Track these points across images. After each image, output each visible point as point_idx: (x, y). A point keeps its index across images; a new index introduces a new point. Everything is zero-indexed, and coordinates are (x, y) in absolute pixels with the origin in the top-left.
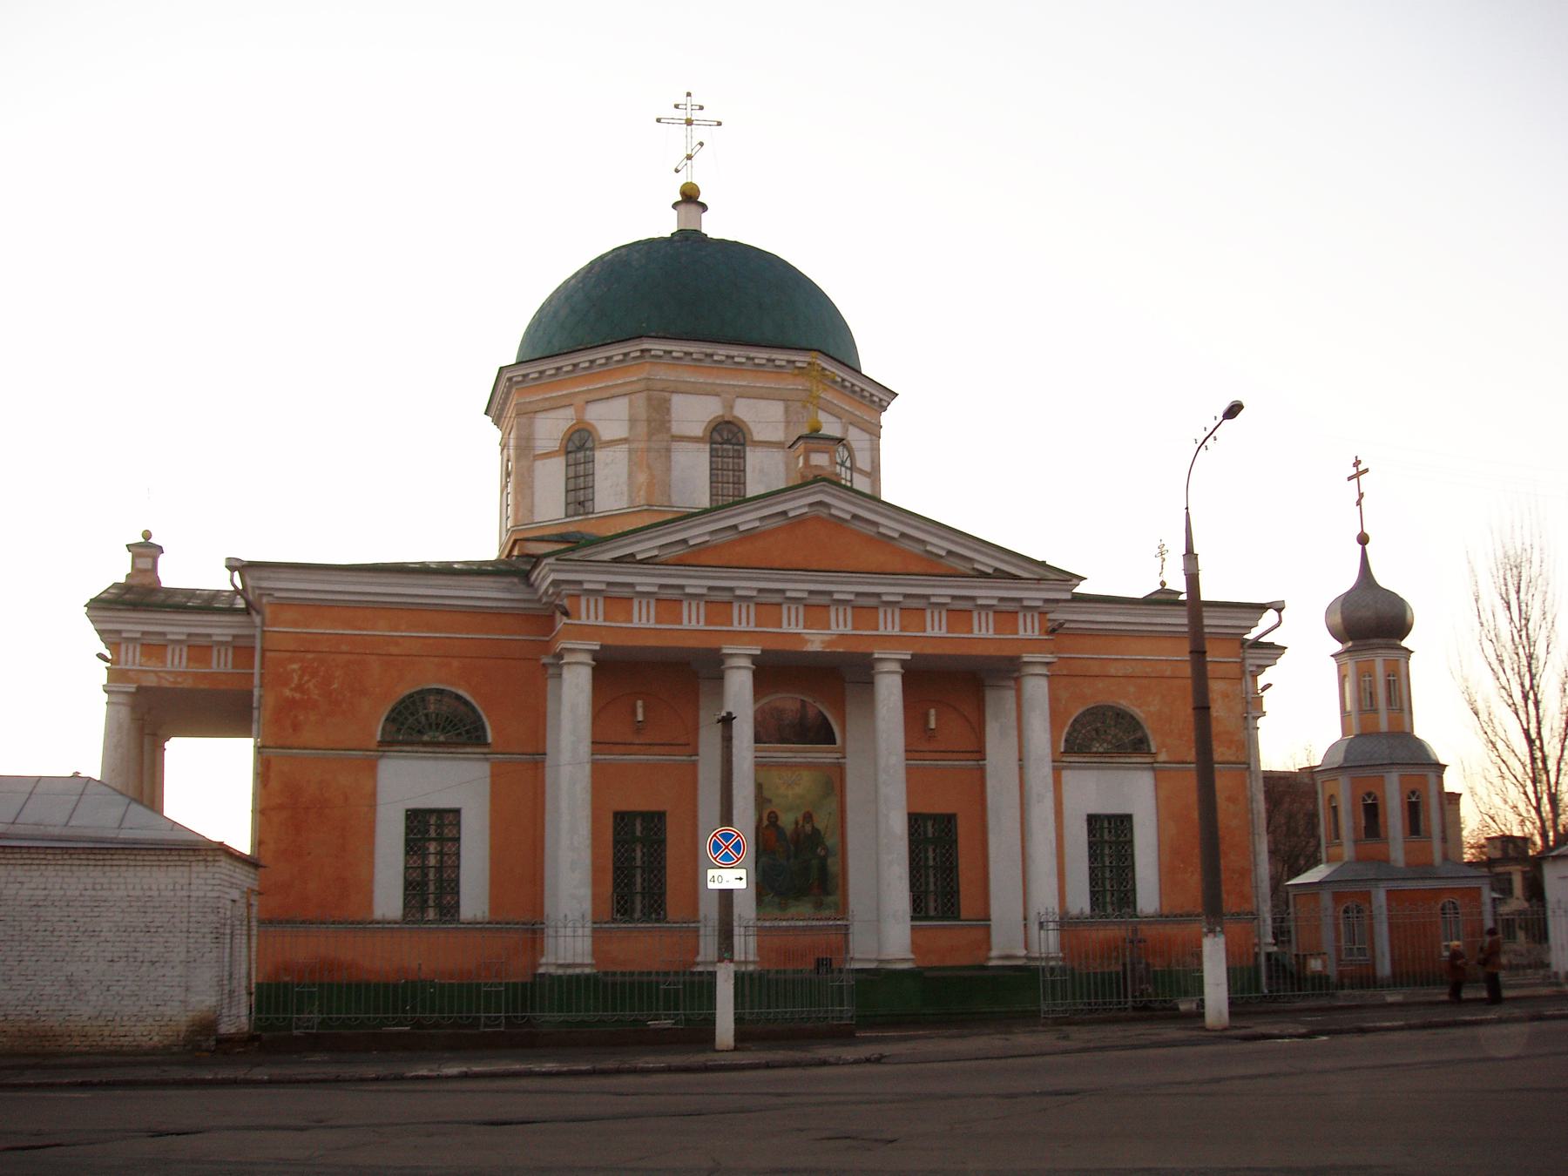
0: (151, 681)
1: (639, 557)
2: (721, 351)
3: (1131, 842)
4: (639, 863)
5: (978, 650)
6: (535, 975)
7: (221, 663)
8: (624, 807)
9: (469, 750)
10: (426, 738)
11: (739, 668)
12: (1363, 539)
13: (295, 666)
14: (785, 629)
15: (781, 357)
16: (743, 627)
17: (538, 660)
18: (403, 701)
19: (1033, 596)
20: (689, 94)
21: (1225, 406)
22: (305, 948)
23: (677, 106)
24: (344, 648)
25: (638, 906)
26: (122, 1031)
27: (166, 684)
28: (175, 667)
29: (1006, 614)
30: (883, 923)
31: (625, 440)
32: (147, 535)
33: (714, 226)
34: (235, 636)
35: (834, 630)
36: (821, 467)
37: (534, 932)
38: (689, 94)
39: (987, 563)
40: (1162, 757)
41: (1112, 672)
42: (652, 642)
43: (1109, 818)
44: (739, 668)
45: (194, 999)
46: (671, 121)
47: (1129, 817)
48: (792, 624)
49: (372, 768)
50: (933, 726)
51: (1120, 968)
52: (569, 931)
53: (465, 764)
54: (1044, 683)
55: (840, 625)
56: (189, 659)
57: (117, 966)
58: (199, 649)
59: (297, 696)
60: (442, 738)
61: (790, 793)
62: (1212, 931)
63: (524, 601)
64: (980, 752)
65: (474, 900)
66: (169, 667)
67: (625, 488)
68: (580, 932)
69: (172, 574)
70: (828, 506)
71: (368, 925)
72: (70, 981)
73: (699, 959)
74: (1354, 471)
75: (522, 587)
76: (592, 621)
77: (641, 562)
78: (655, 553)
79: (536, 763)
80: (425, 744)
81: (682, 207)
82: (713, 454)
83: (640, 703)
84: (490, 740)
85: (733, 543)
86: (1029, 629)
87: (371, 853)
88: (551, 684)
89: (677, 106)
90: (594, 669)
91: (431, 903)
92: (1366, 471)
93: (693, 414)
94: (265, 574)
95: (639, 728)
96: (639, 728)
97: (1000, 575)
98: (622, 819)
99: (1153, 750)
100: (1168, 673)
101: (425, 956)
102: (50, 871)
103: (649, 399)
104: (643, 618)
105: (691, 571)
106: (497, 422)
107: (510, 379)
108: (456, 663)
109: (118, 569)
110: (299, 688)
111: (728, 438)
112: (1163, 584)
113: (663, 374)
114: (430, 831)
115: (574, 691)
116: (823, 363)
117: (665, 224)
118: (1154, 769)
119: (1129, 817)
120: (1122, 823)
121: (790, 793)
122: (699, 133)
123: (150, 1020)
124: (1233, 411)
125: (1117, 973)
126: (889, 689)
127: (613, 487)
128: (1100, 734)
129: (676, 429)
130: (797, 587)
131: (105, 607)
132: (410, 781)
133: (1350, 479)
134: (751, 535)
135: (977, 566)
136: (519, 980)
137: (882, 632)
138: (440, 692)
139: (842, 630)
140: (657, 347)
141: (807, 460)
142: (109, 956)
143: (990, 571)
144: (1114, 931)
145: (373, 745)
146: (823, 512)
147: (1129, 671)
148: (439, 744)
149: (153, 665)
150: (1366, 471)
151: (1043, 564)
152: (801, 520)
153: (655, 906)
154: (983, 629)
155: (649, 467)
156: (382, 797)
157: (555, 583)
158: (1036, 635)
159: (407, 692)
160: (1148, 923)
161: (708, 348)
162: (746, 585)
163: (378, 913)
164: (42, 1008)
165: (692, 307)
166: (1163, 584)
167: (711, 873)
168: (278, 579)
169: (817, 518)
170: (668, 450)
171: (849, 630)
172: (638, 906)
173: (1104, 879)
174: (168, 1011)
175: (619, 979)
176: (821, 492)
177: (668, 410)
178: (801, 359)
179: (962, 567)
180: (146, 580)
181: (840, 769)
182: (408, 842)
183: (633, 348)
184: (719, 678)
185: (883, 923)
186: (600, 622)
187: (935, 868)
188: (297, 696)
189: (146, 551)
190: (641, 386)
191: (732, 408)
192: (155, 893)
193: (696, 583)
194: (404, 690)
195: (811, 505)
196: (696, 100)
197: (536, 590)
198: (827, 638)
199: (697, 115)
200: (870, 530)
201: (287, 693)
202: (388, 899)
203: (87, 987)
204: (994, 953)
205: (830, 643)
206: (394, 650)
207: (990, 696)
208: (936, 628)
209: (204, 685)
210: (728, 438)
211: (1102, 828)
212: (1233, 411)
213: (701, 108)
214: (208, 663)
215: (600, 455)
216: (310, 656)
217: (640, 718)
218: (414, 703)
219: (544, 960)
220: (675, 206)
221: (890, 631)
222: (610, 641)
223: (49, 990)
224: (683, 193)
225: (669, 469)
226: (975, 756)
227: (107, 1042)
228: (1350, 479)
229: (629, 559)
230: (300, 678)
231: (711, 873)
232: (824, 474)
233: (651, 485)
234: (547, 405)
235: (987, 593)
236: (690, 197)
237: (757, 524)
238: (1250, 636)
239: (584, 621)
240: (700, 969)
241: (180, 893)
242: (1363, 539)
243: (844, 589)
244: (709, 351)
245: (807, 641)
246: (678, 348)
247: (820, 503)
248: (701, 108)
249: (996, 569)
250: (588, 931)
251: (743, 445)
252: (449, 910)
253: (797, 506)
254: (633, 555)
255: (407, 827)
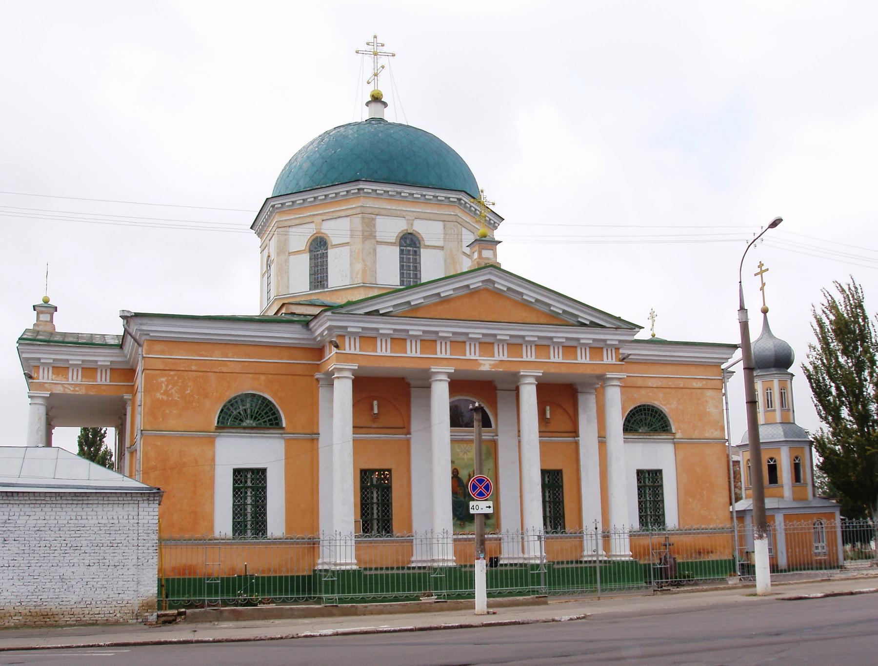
0: (58, 390)
1: (381, 312)
2: (406, 191)
3: (662, 486)
4: (375, 500)
5: (580, 371)
6: (314, 571)
7: (103, 379)
8: (366, 467)
9: (271, 431)
10: (244, 424)
11: (440, 380)
12: (765, 311)
13: (163, 379)
14: (468, 357)
15: (442, 195)
16: (443, 356)
17: (313, 376)
18: (230, 401)
19: (613, 338)
20: (375, 37)
21: (771, 220)
22: (183, 558)
23: (368, 44)
24: (194, 368)
25: (375, 527)
26: (97, 611)
27: (69, 392)
28: (73, 383)
29: (597, 349)
30: (525, 536)
31: (442, 248)
32: (46, 301)
33: (390, 115)
34: (111, 362)
35: (497, 358)
36: (488, 259)
37: (313, 545)
38: (375, 37)
39: (585, 318)
40: (678, 435)
41: (650, 385)
42: (389, 364)
43: (649, 471)
44: (440, 380)
45: (142, 589)
46: (364, 53)
47: (660, 471)
48: (472, 354)
49: (212, 441)
50: (548, 416)
51: (731, 558)
52: (343, 542)
53: (270, 441)
54: (617, 391)
55: (501, 354)
56: (82, 377)
57: (93, 569)
58: (89, 370)
59: (165, 398)
60: (254, 424)
61: (465, 457)
62: (761, 537)
63: (304, 339)
64: (575, 432)
65: (276, 522)
66: (70, 382)
67: (348, 273)
68: (349, 543)
69: (63, 324)
70: (494, 282)
71: (210, 542)
72: (62, 579)
73: (413, 559)
74: (759, 270)
75: (304, 331)
76: (352, 351)
77: (383, 315)
78: (391, 309)
79: (313, 440)
80: (245, 428)
81: (373, 105)
82: (402, 251)
83: (375, 403)
84: (284, 425)
85: (436, 304)
86: (609, 359)
87: (212, 496)
88: (322, 392)
89: (368, 44)
90: (354, 381)
91: (249, 526)
92: (767, 270)
93: (390, 228)
94: (145, 320)
95: (375, 418)
96: (375, 418)
97: (594, 325)
98: (365, 474)
99: (674, 431)
100: (681, 386)
101: (248, 559)
102: (48, 509)
103: (363, 218)
104: (383, 350)
105: (415, 321)
106: (259, 234)
107: (273, 206)
108: (263, 377)
109: (29, 320)
110: (166, 393)
111: (410, 244)
112: (653, 336)
113: (370, 203)
114: (250, 483)
115: (343, 392)
116: (465, 199)
117: (362, 114)
118: (674, 443)
119: (660, 471)
120: (771, 483)
121: (465, 457)
122: (383, 60)
123: (114, 603)
124: (774, 224)
125: (729, 560)
126: (529, 396)
127: (341, 272)
128: (645, 421)
129: (380, 236)
130: (476, 331)
131: (27, 341)
132: (239, 451)
133: (755, 275)
134: (447, 300)
135: (580, 320)
136: (306, 573)
137: (525, 359)
138: (254, 395)
139: (502, 358)
140: (368, 187)
141: (480, 254)
142: (87, 562)
143: (588, 323)
144: (655, 538)
145: (213, 428)
146: (490, 286)
147: (659, 384)
148: (252, 428)
149: (60, 380)
150: (767, 270)
151: (619, 319)
152: (475, 292)
153: (386, 526)
154: (583, 358)
155: (363, 260)
156: (218, 460)
157: (330, 328)
158: (614, 362)
159: (233, 396)
160: (673, 534)
161: (399, 189)
162: (446, 330)
163: (217, 534)
164: (44, 596)
165: (386, 161)
166: (653, 336)
167: (472, 503)
168: (151, 325)
169: (486, 290)
170: (375, 250)
171: (505, 358)
172: (375, 527)
173: (646, 508)
174: (125, 597)
175: (272, 575)
176: (490, 273)
177: (374, 226)
178: (454, 196)
179: (572, 320)
180: (48, 328)
181: (495, 443)
182: (234, 489)
183: (353, 188)
184: (428, 387)
185: (525, 536)
186: (358, 352)
187: (550, 502)
188: (165, 398)
189: (46, 309)
190: (358, 211)
191: (412, 224)
192: (116, 521)
193: (416, 328)
194: (231, 394)
195: (483, 282)
196: (380, 40)
197: (313, 333)
198: (493, 362)
199: (380, 49)
200: (517, 298)
201: (158, 396)
202: (223, 522)
203: (73, 583)
204: (585, 553)
205: (495, 366)
206: (225, 369)
207: (581, 398)
208: (556, 357)
209: (92, 393)
210: (410, 244)
211: (644, 478)
212: (774, 224)
213: (383, 45)
214: (95, 379)
215: (330, 252)
216: (172, 373)
217: (376, 411)
218: (236, 402)
219: (320, 561)
220: (367, 104)
221: (529, 359)
222: (364, 363)
223: (48, 585)
224: (373, 96)
225: (375, 262)
226: (573, 434)
227: (87, 618)
228: (755, 275)
229: (376, 313)
230: (167, 386)
231: (472, 503)
232: (491, 262)
233: (364, 271)
234: (297, 222)
235: (587, 336)
236: (376, 99)
237: (452, 292)
238: (723, 367)
239: (347, 351)
240: (413, 565)
241: (132, 521)
242: (765, 311)
243: (504, 333)
244: (399, 190)
245: (481, 364)
246: (380, 188)
247: (489, 281)
248: (383, 45)
249: (591, 322)
250: (353, 542)
251: (419, 247)
252: (260, 525)
253: (475, 282)
254: (377, 311)
255: (234, 480)
